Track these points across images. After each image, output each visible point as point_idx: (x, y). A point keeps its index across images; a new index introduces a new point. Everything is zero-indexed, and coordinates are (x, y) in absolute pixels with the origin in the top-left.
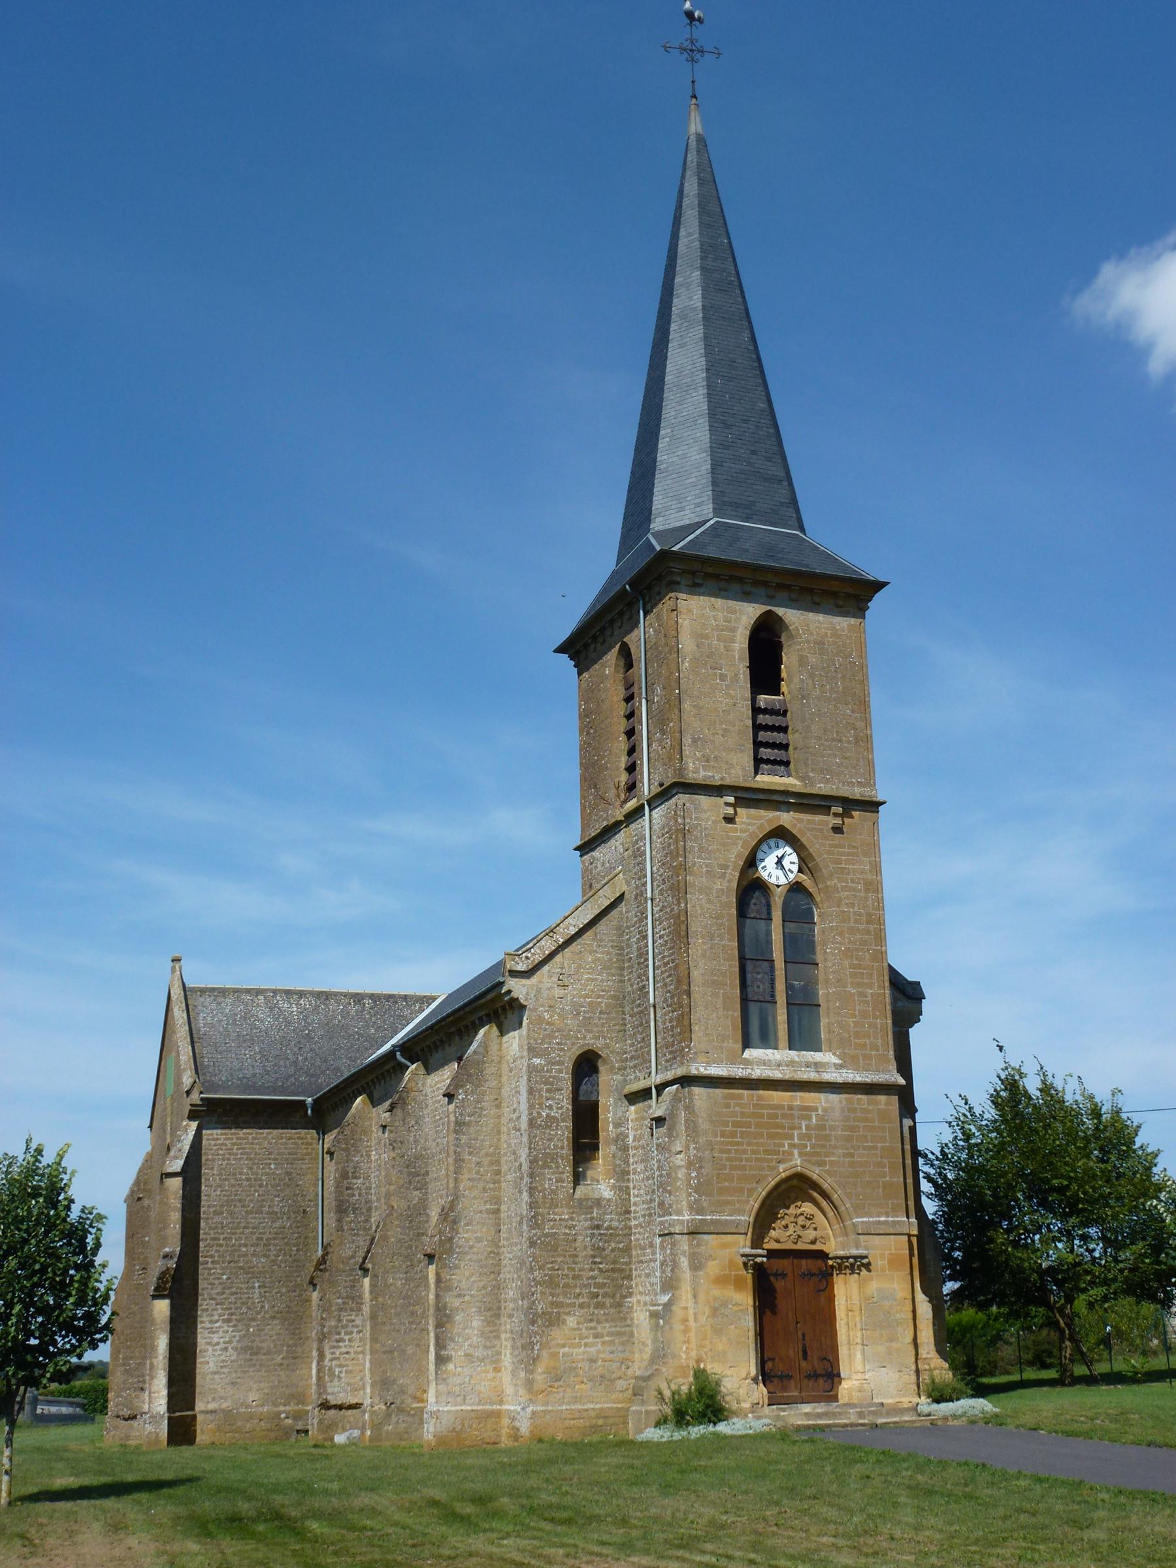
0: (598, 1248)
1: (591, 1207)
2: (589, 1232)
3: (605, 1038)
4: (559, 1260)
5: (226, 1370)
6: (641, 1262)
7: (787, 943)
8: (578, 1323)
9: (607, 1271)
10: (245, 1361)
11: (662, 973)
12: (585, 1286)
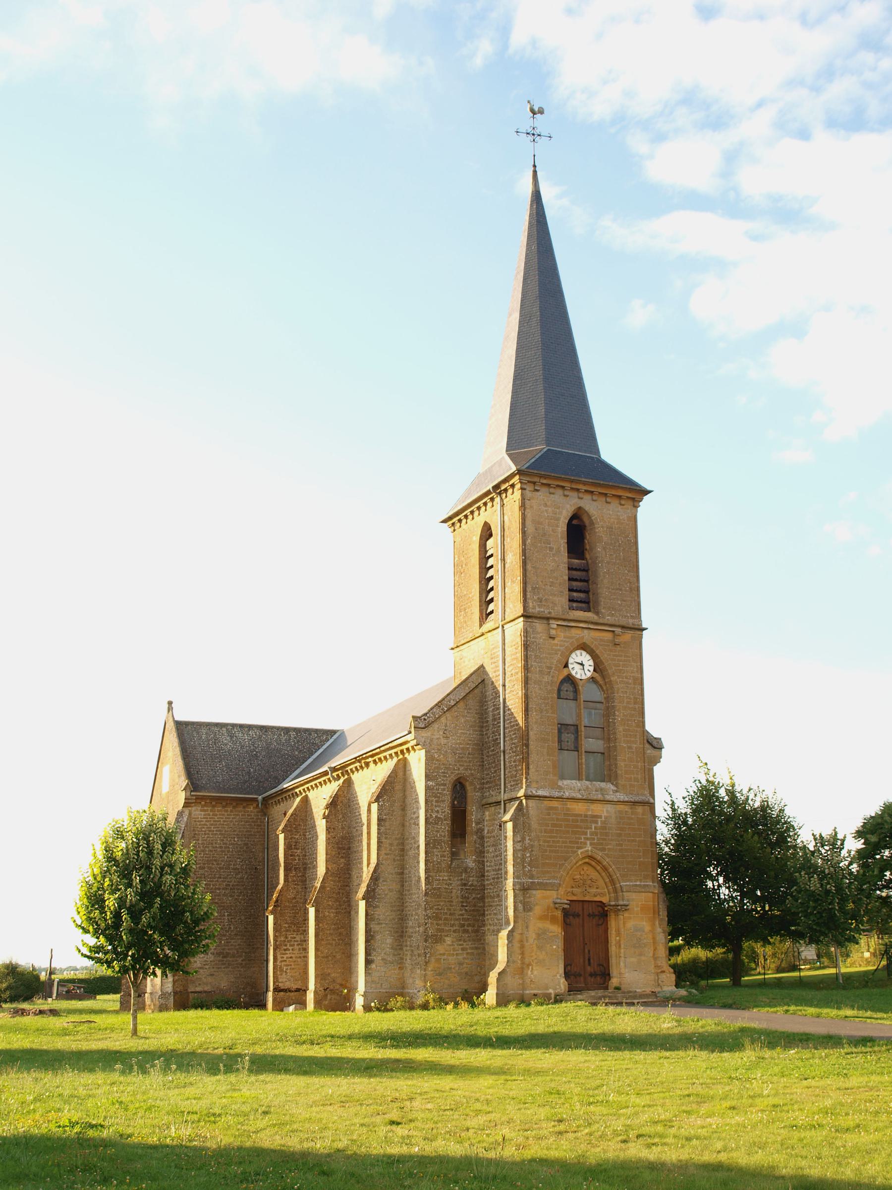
0: (465, 897)
1: (461, 873)
2: (460, 887)
3: (471, 770)
4: (442, 904)
5: (207, 967)
6: (491, 906)
7: (534, 688)
8: (452, 942)
9: (470, 911)
10: (219, 961)
11: (509, 732)
12: (457, 920)
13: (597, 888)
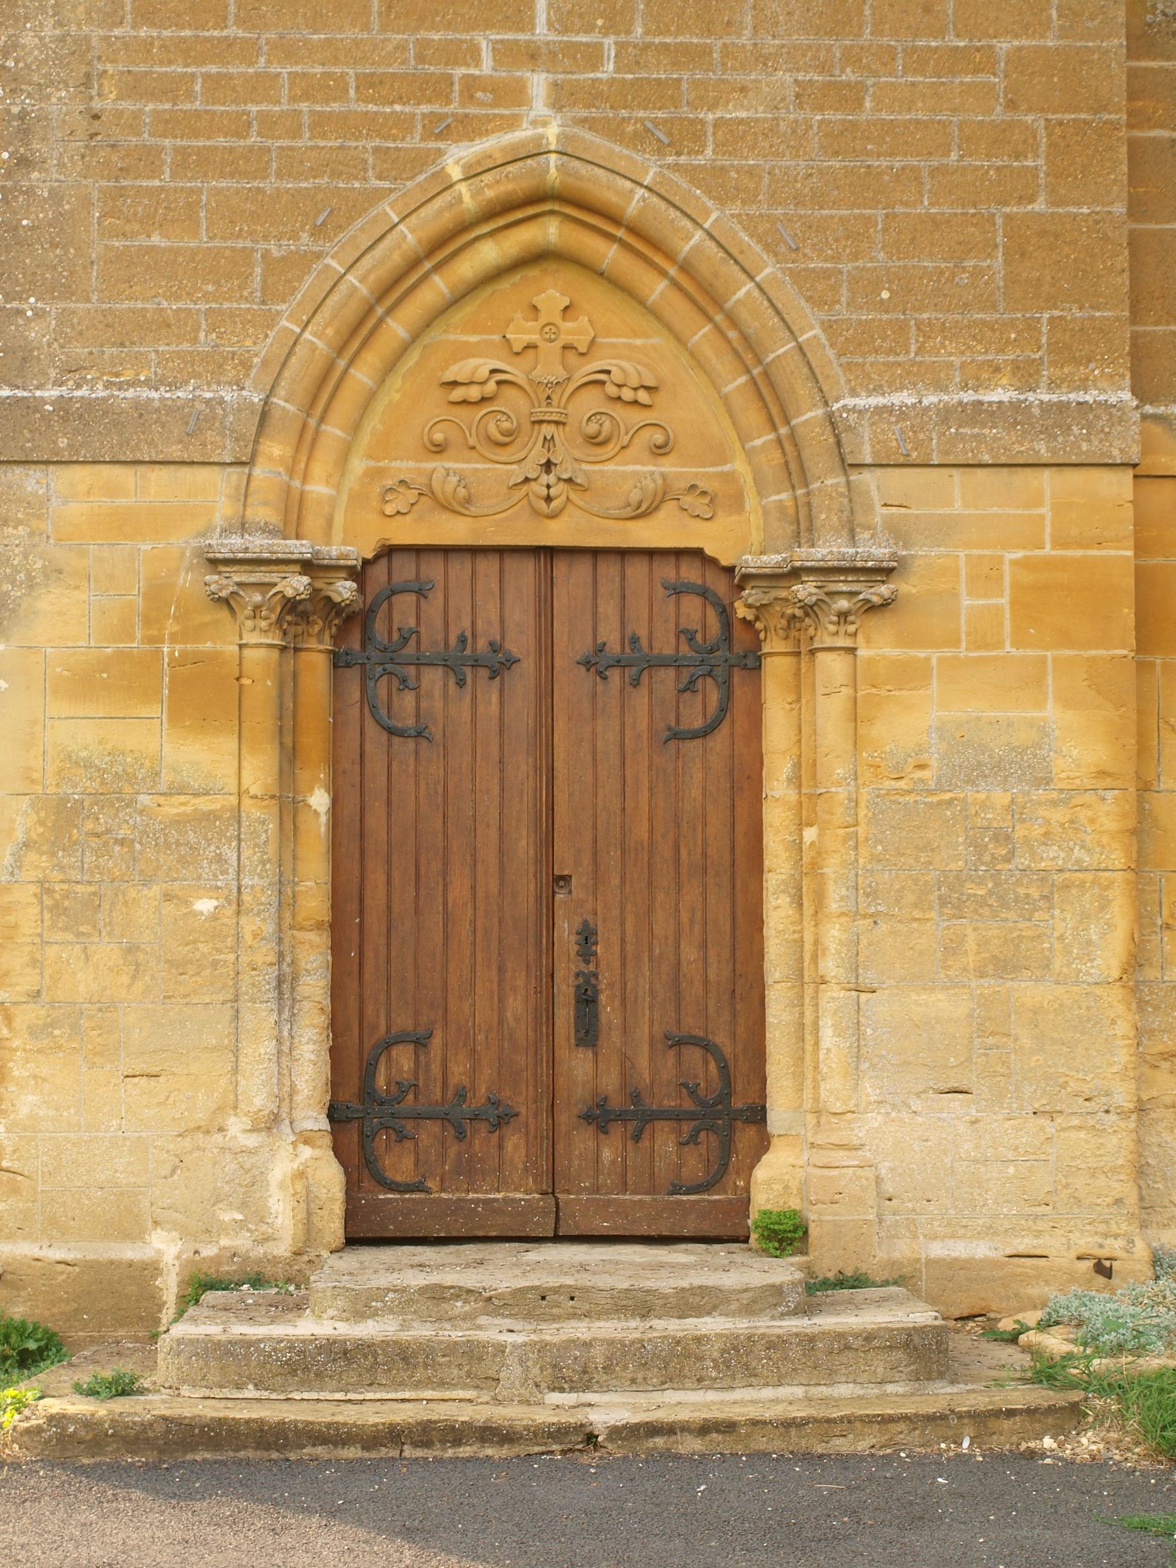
13: (660, 450)
